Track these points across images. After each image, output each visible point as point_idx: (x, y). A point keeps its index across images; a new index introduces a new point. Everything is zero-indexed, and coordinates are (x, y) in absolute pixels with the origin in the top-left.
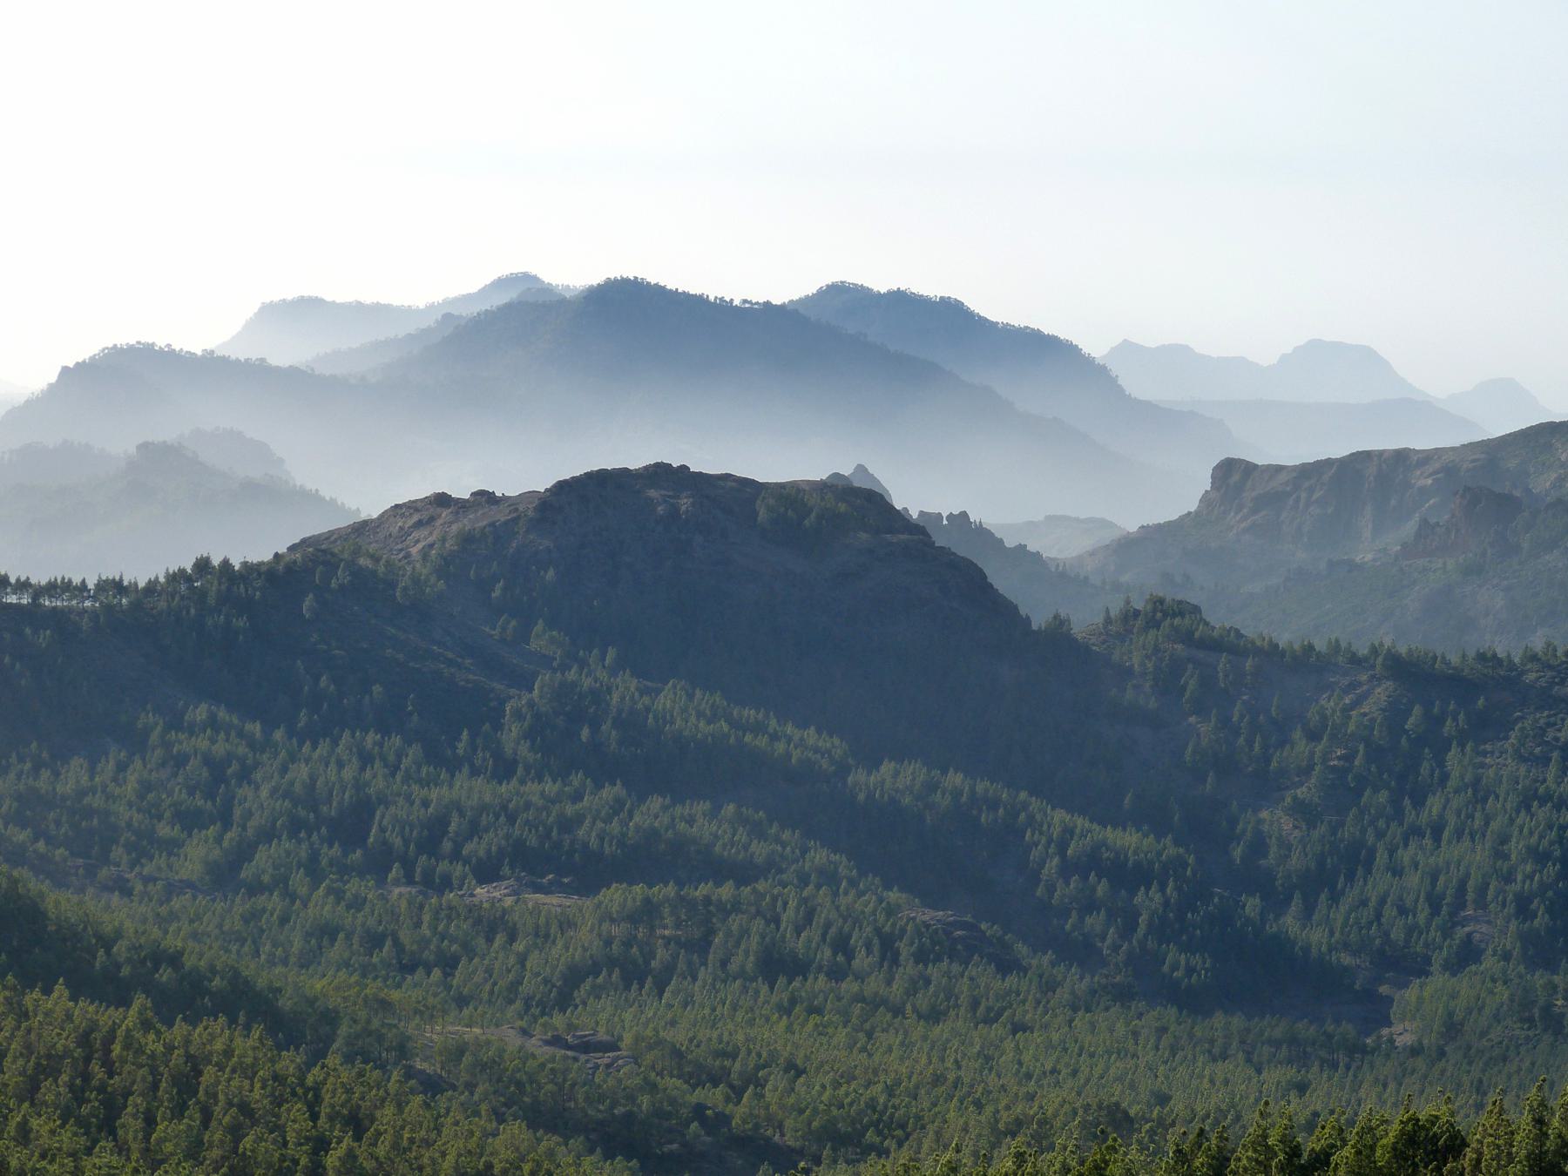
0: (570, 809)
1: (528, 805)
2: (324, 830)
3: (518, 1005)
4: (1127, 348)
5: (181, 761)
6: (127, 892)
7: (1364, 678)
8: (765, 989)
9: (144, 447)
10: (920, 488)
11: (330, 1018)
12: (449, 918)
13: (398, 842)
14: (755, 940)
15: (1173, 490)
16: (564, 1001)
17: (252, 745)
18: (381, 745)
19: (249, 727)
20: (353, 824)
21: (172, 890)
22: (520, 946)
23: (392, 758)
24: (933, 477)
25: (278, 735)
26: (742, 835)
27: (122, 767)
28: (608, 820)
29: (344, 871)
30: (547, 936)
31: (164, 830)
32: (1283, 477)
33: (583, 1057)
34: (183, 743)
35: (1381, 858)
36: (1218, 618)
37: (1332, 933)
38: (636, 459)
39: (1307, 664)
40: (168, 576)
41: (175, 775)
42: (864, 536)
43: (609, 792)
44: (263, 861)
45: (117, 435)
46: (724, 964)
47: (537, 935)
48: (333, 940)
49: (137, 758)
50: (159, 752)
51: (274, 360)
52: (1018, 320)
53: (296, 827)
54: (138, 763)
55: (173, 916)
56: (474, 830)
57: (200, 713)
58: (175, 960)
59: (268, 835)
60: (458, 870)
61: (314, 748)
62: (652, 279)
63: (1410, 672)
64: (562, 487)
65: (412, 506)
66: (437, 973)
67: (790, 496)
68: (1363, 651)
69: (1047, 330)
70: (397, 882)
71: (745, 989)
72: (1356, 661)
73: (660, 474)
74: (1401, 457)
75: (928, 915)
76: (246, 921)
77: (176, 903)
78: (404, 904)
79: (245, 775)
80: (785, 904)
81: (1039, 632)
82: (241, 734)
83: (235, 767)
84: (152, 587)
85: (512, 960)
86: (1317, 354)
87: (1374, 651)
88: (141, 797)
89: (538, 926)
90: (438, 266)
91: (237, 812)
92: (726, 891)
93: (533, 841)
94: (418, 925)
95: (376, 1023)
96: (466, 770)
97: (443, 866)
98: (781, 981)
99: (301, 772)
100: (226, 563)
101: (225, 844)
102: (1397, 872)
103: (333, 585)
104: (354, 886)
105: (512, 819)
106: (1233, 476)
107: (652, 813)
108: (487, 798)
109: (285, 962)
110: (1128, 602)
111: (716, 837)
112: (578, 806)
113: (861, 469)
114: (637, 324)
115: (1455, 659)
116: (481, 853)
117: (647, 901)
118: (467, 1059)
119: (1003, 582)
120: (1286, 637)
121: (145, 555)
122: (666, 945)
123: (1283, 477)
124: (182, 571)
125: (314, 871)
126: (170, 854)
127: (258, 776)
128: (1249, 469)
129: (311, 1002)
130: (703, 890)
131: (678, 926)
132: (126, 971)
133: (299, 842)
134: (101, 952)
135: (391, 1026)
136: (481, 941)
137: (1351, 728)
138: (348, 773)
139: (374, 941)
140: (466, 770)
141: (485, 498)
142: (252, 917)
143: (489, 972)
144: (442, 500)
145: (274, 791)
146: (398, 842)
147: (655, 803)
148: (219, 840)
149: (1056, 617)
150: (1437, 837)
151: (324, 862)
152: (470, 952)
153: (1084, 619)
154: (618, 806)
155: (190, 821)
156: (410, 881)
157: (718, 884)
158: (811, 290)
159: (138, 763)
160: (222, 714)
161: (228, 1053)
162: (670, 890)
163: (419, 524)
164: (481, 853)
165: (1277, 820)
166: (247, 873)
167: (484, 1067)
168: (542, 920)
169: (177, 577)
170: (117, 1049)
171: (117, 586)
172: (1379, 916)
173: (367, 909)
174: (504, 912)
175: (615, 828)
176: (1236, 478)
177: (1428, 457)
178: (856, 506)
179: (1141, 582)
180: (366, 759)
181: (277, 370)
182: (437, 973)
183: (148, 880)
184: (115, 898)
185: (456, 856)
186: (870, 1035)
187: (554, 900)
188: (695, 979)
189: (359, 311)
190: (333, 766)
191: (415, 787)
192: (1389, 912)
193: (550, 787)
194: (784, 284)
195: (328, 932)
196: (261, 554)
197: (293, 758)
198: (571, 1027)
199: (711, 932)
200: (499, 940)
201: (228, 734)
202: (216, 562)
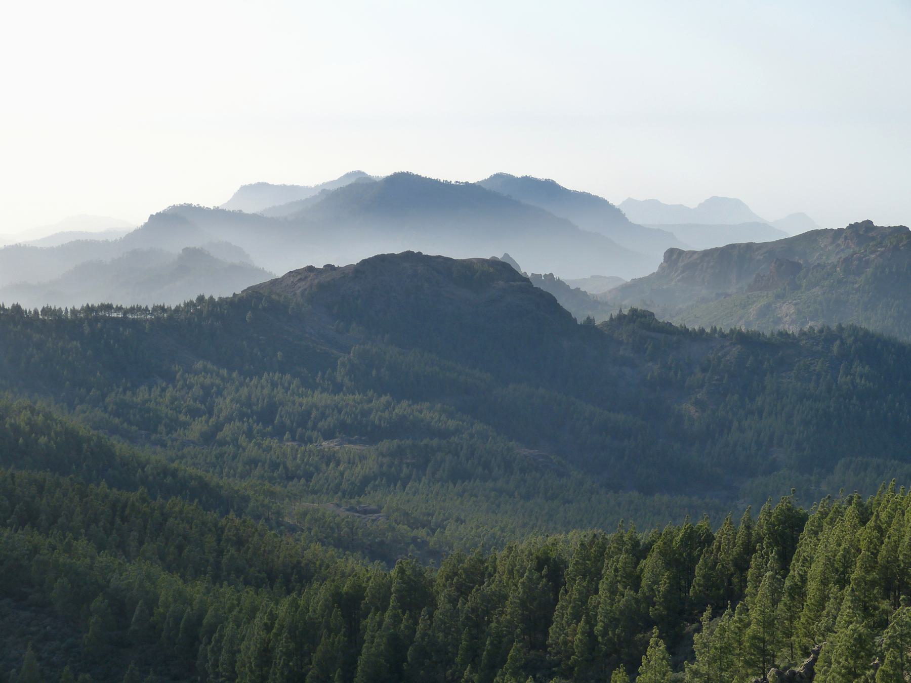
0: (366, 407)
1: (347, 404)
2: (255, 417)
3: (340, 494)
4: (630, 201)
5: (190, 387)
6: (164, 445)
7: (727, 344)
8: (451, 486)
9: (186, 250)
10: (532, 262)
11: (246, 499)
12: (310, 456)
13: (288, 422)
17: (223, 379)
18: (281, 379)
20: (267, 415)
22: (341, 468)
23: (286, 385)
25: (235, 375)
26: (444, 417)
27: (163, 390)
28: (384, 411)
29: (264, 435)
30: (354, 463)
31: (182, 418)
32: (696, 256)
33: (363, 516)
35: (736, 424)
36: (662, 317)
38: (397, 248)
39: (699, 336)
40: (185, 304)
42: (501, 283)
43: (384, 399)
44: (227, 431)
45: (174, 245)
47: (349, 463)
48: (256, 466)
50: (181, 383)
51: (245, 211)
52: (580, 189)
53: (242, 416)
54: (171, 388)
55: (183, 457)
56: (323, 416)
57: (199, 365)
58: (174, 473)
59: (229, 419)
60: (315, 434)
61: (251, 379)
62: (415, 171)
64: (365, 262)
65: (297, 272)
66: (303, 481)
67: (467, 266)
68: (727, 331)
70: (288, 440)
71: (443, 486)
72: (723, 336)
73: (409, 256)
74: (749, 246)
76: (217, 458)
77: (186, 450)
78: (289, 450)
79: (219, 393)
80: (462, 448)
81: (581, 325)
82: (218, 375)
84: (177, 309)
85: (337, 474)
86: (714, 203)
88: (172, 403)
89: (349, 459)
90: (318, 168)
91: (216, 410)
92: (435, 442)
93: (349, 421)
94: (295, 459)
95: (266, 501)
96: (320, 389)
97: (309, 433)
98: (459, 481)
99: (245, 391)
100: (211, 298)
103: (260, 307)
104: (266, 442)
105: (340, 411)
106: (673, 256)
107: (403, 408)
109: (234, 476)
110: (621, 311)
111: (432, 418)
112: (370, 405)
113: (506, 255)
114: (406, 194)
115: (768, 334)
118: (308, 517)
119: (564, 302)
121: (175, 296)
122: (408, 467)
123: (696, 256)
124: (191, 302)
125: (250, 435)
126: (185, 429)
127: (225, 393)
128: (680, 253)
129: (237, 492)
132: (151, 478)
133: (243, 422)
134: (140, 470)
135: (273, 503)
136: (324, 467)
137: (722, 366)
139: (275, 466)
140: (320, 389)
141: (329, 268)
142: (220, 456)
143: (327, 479)
144: (310, 269)
145: (232, 400)
147: (405, 403)
148: (207, 422)
149: (588, 318)
151: (255, 431)
152: (317, 469)
153: (600, 319)
154: (388, 405)
155: (194, 413)
156: (294, 440)
158: (487, 177)
159: (171, 388)
160: (210, 366)
161: (181, 512)
165: (689, 409)
166: (220, 436)
167: (316, 520)
168: (352, 456)
169: (189, 305)
170: (127, 511)
171: (163, 309)
173: (272, 452)
175: (386, 415)
176: (675, 256)
178: (502, 270)
179: (627, 305)
180: (274, 385)
181: (247, 215)
182: (303, 481)
183: (173, 440)
184: (158, 449)
185: (314, 428)
186: (498, 506)
187: (358, 447)
188: (420, 481)
189: (284, 188)
190: (259, 388)
191: (296, 398)
193: (358, 397)
195: (253, 462)
196: (228, 294)
197: (241, 385)
198: (359, 503)
200: (332, 465)
201: (212, 374)
202: (207, 297)
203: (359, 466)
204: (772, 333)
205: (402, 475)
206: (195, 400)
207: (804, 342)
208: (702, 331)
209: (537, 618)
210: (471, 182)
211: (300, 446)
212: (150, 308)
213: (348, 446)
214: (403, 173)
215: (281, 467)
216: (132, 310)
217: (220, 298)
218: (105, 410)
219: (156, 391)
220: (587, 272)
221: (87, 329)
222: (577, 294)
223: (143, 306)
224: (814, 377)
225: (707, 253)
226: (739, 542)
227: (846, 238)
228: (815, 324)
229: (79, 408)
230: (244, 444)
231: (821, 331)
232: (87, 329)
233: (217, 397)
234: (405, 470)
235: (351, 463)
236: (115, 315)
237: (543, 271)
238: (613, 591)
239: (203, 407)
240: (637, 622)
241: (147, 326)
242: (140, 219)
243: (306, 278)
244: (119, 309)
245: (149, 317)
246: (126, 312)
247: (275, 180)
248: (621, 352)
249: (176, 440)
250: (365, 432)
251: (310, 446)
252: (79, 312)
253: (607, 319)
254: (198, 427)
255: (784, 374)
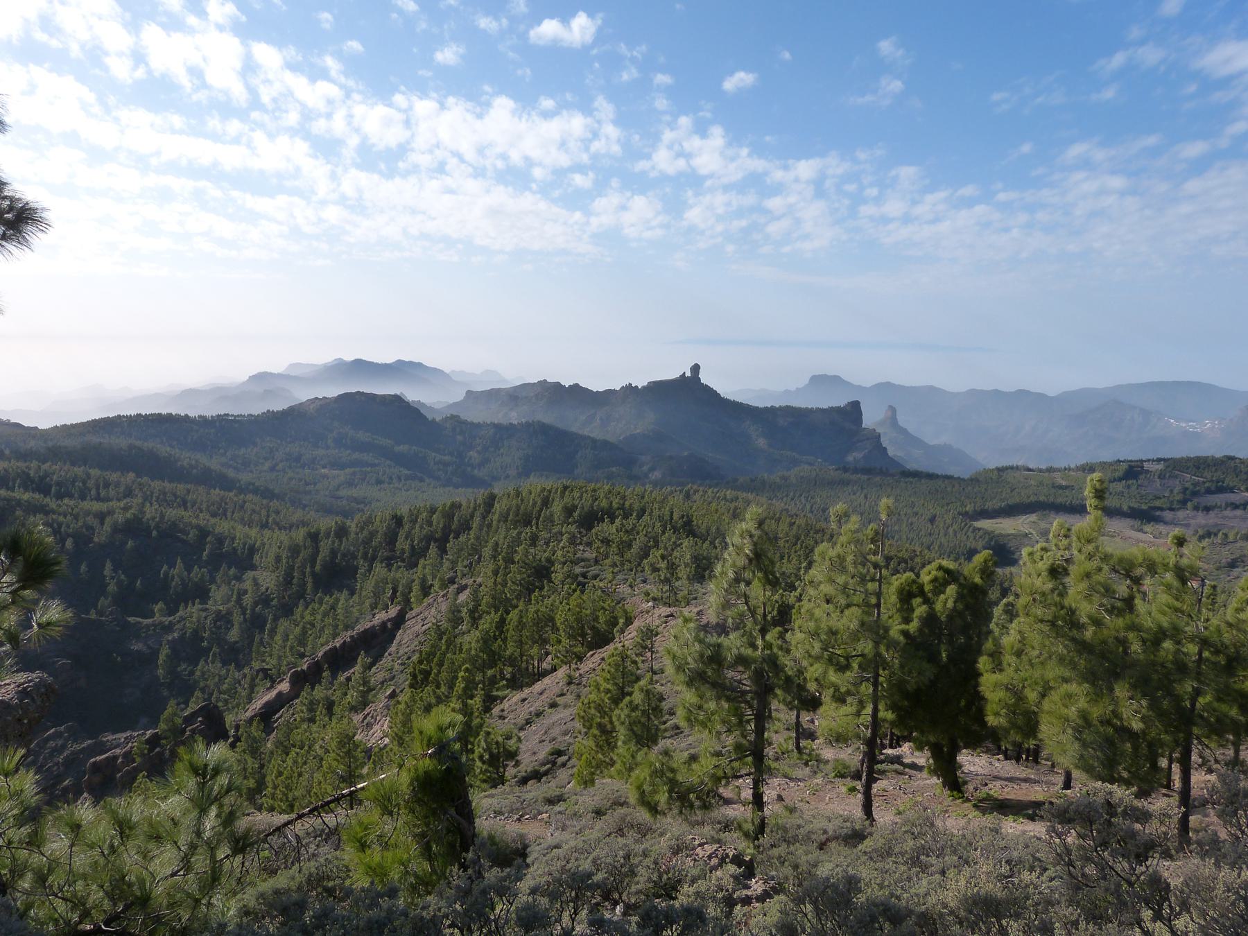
10: (412, 394)
44: (280, 466)
90: (324, 355)
106: (469, 393)
107: (356, 455)
114: (361, 367)
139: (300, 480)
155: (266, 459)
178: (397, 400)
196: (280, 409)
209: (391, 539)
220: (430, 398)
238: (421, 527)
240: (429, 539)
248: (885, 502)
250: (336, 464)
254: (267, 465)
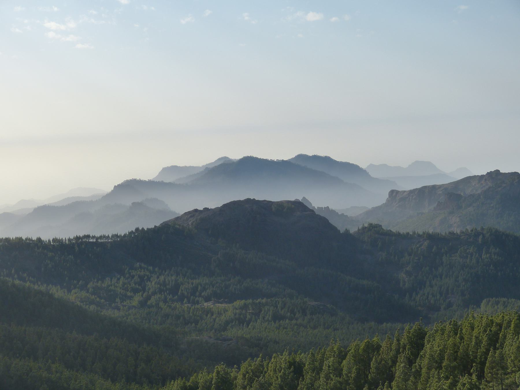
3: (213, 331)
4: (371, 166)
5: (133, 277)
6: (119, 309)
7: (422, 240)
8: (273, 324)
9: (133, 204)
14: (271, 311)
15: (378, 198)
16: (225, 329)
19: (149, 268)
21: (130, 308)
22: (214, 317)
24: (320, 198)
25: (156, 269)
27: (119, 279)
30: (221, 314)
31: (129, 294)
32: (406, 193)
34: (133, 273)
37: (416, 302)
38: (242, 198)
39: (406, 237)
41: (132, 280)
44: (153, 301)
45: (128, 201)
46: (264, 318)
49: (122, 277)
51: (165, 181)
52: (344, 160)
59: (154, 293)
60: (200, 299)
61: (165, 272)
62: (254, 156)
63: (433, 238)
64: (225, 205)
66: (193, 325)
67: (280, 205)
68: (421, 233)
69: (351, 162)
70: (186, 303)
72: (419, 236)
73: (248, 201)
75: (314, 303)
77: (130, 312)
78: (186, 308)
79: (149, 279)
80: (279, 302)
83: (146, 277)
84: (125, 235)
85: (212, 320)
87: (424, 233)
90: (204, 156)
91: (147, 289)
92: (264, 301)
94: (189, 313)
97: (197, 299)
98: (277, 321)
99: (162, 278)
100: (143, 229)
101: (144, 296)
102: (431, 286)
106: (393, 193)
108: (207, 281)
110: (363, 225)
113: (304, 198)
114: (250, 167)
115: (444, 234)
116: (206, 295)
117: (245, 304)
119: (333, 222)
120: (402, 231)
121: (123, 229)
123: (406, 193)
124: (132, 231)
125: (165, 301)
127: (152, 279)
128: (398, 192)
130: (259, 300)
131: (253, 309)
133: (162, 295)
136: (205, 316)
137: (419, 252)
138: (173, 278)
141: (206, 209)
143: (206, 323)
144: (196, 211)
145: (155, 283)
146: (186, 293)
148: (142, 295)
149: (346, 230)
150: (441, 278)
153: (353, 230)
155: (135, 291)
156: (189, 302)
157: (262, 299)
158: (294, 156)
160: (143, 265)
162: (250, 301)
163: (191, 217)
164: (206, 295)
165: (402, 275)
166: (149, 303)
171: (117, 236)
172: (428, 297)
174: (210, 309)
176: (394, 194)
177: (440, 186)
178: (299, 206)
182: (193, 325)
183: (124, 306)
185: (200, 296)
187: (223, 305)
188: (257, 322)
192: (430, 296)
194: (287, 155)
197: (160, 275)
199: (261, 311)
200: (209, 315)
202: (140, 228)
203: (224, 316)
204: (446, 233)
205: (247, 319)
206: (135, 284)
207: (463, 237)
208: (408, 233)
210: (285, 159)
211: (192, 306)
212: (110, 236)
213: (217, 305)
214: (248, 157)
215: (182, 318)
216: (101, 237)
217: (147, 229)
218: (88, 292)
219: (114, 280)
221: (77, 249)
222: (343, 216)
223: (107, 235)
224: (469, 256)
225: (411, 192)
226: (394, 348)
227: (486, 180)
228: (469, 228)
229: (73, 291)
230: (162, 307)
231: (472, 231)
232: (77, 249)
233: (147, 282)
234: (248, 317)
235: (220, 314)
236: (91, 240)
237: (324, 205)
239: (140, 287)
241: (109, 245)
242: (109, 188)
243: (194, 215)
244: (94, 237)
245: (110, 240)
246: (97, 238)
247: (181, 163)
249: (125, 306)
251: (198, 306)
252: (72, 240)
253: (357, 230)
255: (453, 255)
